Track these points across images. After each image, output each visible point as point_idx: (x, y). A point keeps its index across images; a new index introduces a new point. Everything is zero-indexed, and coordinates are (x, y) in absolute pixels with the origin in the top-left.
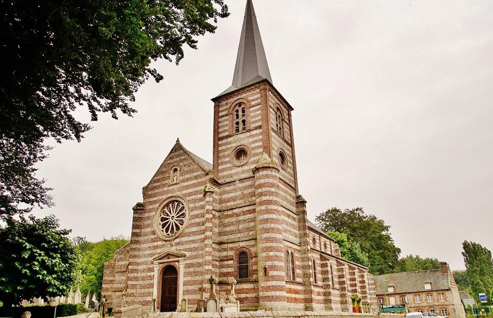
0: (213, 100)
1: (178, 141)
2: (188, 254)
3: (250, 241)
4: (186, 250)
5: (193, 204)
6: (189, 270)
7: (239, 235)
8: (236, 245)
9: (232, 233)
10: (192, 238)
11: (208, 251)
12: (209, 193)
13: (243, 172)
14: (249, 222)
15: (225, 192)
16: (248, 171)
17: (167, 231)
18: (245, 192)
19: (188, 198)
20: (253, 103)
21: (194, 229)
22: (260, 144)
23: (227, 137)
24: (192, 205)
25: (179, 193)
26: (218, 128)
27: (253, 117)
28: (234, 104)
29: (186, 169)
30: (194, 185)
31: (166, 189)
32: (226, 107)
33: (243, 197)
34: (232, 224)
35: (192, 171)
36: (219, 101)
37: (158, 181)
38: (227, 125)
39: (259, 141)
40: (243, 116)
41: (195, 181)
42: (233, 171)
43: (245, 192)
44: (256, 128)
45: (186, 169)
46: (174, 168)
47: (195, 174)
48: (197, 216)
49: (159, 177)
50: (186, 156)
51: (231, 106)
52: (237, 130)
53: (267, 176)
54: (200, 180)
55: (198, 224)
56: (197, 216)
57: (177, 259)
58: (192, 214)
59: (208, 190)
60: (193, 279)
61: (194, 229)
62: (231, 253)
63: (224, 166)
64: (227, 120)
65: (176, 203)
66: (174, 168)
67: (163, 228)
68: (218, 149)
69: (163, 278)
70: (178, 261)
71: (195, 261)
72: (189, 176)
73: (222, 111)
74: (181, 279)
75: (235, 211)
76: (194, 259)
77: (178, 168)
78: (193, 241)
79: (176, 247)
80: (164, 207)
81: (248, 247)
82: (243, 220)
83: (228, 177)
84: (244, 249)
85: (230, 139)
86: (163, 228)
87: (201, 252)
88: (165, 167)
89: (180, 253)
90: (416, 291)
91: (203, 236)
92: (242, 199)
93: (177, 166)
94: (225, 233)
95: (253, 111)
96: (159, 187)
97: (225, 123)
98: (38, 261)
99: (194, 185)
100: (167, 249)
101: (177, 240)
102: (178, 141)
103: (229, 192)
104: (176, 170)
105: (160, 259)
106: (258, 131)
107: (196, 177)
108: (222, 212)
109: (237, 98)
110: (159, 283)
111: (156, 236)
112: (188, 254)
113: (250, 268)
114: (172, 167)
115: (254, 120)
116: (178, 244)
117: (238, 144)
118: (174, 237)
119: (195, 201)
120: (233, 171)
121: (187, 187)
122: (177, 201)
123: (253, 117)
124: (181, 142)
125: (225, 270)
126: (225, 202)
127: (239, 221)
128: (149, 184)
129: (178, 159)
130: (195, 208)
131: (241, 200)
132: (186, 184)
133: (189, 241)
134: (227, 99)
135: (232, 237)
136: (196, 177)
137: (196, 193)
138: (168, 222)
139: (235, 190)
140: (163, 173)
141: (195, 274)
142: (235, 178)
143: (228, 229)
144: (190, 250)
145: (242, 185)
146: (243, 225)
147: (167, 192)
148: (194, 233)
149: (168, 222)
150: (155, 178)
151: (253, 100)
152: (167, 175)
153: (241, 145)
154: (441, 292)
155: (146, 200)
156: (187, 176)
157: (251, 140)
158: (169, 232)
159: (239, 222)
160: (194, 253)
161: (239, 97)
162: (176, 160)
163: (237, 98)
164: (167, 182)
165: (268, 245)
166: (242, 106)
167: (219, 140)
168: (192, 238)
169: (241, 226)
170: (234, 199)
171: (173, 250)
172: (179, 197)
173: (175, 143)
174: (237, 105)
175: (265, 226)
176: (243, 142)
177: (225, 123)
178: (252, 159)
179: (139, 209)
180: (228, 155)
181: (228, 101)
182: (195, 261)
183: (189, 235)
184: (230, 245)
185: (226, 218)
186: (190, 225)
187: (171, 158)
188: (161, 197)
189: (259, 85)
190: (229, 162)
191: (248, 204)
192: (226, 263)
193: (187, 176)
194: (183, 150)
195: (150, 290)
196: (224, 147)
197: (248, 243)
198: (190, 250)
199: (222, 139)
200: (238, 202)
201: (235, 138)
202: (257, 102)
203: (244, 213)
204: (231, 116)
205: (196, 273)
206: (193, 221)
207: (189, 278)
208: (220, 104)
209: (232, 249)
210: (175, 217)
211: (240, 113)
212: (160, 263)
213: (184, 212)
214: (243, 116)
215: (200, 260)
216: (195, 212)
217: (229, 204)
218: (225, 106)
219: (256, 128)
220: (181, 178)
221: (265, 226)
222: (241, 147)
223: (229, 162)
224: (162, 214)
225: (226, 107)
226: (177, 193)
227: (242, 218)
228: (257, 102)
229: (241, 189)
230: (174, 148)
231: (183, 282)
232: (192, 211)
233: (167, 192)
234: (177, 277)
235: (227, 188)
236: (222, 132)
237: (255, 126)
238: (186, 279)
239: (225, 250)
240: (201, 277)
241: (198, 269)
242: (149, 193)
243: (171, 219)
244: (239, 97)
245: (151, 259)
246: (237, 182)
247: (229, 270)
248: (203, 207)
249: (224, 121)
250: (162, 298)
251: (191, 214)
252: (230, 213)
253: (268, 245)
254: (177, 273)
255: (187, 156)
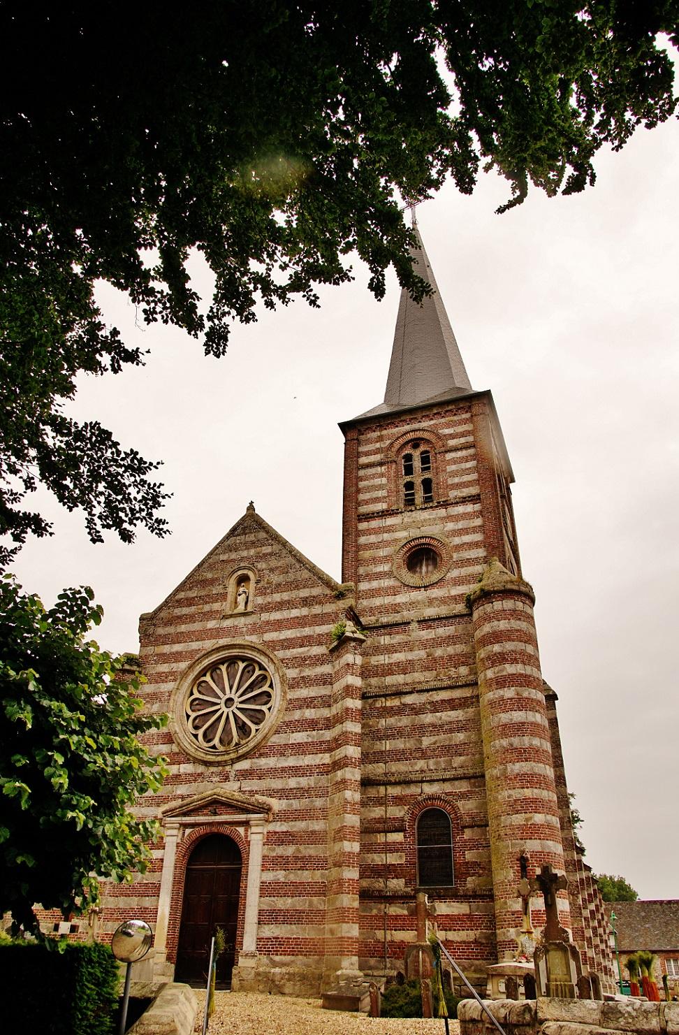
0: (345, 427)
1: (251, 507)
2: (276, 804)
3: (456, 783)
4: (271, 793)
5: (297, 670)
6: (280, 851)
7: (421, 764)
8: (414, 790)
9: (399, 756)
10: (291, 762)
11: (349, 799)
12: (353, 644)
13: (431, 602)
14: (451, 731)
15: (378, 650)
16: (455, 599)
17: (207, 738)
18: (439, 652)
19: (281, 654)
20: (452, 443)
21: (299, 737)
22: (478, 537)
23: (383, 514)
24: (292, 673)
25: (253, 639)
26: (358, 491)
27: (454, 474)
28: (401, 441)
29: (276, 578)
30: (301, 622)
31: (211, 624)
32: (378, 445)
33: (431, 664)
34: (398, 733)
35: (296, 586)
36: (359, 430)
37: (190, 602)
38: (380, 487)
39: (474, 530)
40: (423, 469)
41: (305, 611)
42: (400, 599)
43: (439, 652)
44: (464, 500)
45: (276, 578)
46: (240, 573)
47: (304, 593)
48: (309, 703)
49: (191, 594)
50: (276, 548)
51: (392, 444)
52: (410, 502)
53: (499, 615)
54: (317, 610)
55: (312, 725)
56: (309, 703)
57: (243, 817)
58: (292, 695)
59: (351, 635)
60: (292, 877)
61: (299, 737)
62: (396, 812)
63: (375, 584)
64: (382, 475)
65: (242, 665)
66: (240, 573)
67: (196, 728)
68: (356, 541)
69: (188, 870)
70: (246, 824)
71: (300, 825)
72: (286, 596)
73: (367, 454)
74: (255, 876)
75: (408, 699)
76: (295, 819)
77: (251, 574)
78: (296, 771)
79: (237, 785)
80: (203, 673)
81: (450, 798)
82: (434, 726)
83: (387, 612)
84: (437, 802)
85: (390, 521)
86: (196, 728)
87: (319, 803)
88: (211, 568)
89: (253, 799)
90: (668, 948)
91: (326, 758)
92: (427, 669)
93: (249, 569)
94: (380, 757)
95: (454, 461)
96: (191, 618)
97: (377, 481)
98: (63, 748)
99: (301, 622)
100: (211, 786)
101: (244, 765)
102: (251, 507)
103: (391, 649)
104: (243, 579)
105: (185, 814)
106: (470, 508)
107: (306, 602)
108: (370, 701)
109: (407, 428)
110: (175, 883)
111: (175, 748)
112: (276, 804)
113: (457, 858)
114: (234, 572)
115: (456, 480)
116: (245, 775)
117: (415, 533)
118: (233, 756)
119: (301, 662)
120: (400, 599)
121: (279, 625)
122: (243, 659)
123: (454, 474)
124: (259, 511)
125: (378, 859)
126: (376, 675)
127: (422, 727)
128: (160, 609)
129: (252, 552)
130: (305, 681)
131: (427, 674)
132: (276, 616)
133: (283, 770)
134: (381, 427)
135: (398, 767)
136: (306, 602)
137: (319, 640)
138: (217, 711)
139: (408, 646)
140: (205, 583)
141: (300, 864)
142: (406, 615)
143: (388, 745)
144: (283, 794)
145: (426, 634)
146: (433, 739)
147: (218, 633)
148: (300, 749)
149: (217, 711)
150: (182, 595)
151: (452, 436)
152: (216, 590)
153: (423, 537)
154: (672, 955)
155: (150, 650)
156: (277, 597)
157: (450, 526)
158: (216, 741)
159: (421, 730)
160: (296, 804)
161: (416, 426)
162: (245, 554)
163: (407, 428)
164: (216, 606)
165: (528, 793)
166: (422, 448)
167: (360, 520)
168: (291, 762)
169: (426, 741)
170: (404, 668)
171: (230, 789)
172: (253, 648)
173: (244, 512)
174: (407, 443)
175: (516, 741)
176: (428, 530)
177: (377, 481)
178: (455, 573)
179: (532, 589)
180: (386, 559)
181: (384, 432)
182: (300, 825)
183: (282, 751)
184: (394, 791)
185: (380, 716)
186: (287, 724)
187: (230, 549)
188: (195, 645)
189: (468, 404)
190: (389, 574)
191: (447, 683)
192: (381, 838)
193: (277, 597)
194: (267, 532)
195: (147, 902)
196: (373, 539)
197: (448, 787)
198: (283, 794)
199: (368, 517)
200: (418, 676)
201: (407, 517)
202: (463, 440)
203: (436, 707)
204: (394, 466)
205: (303, 863)
206: (297, 715)
207: (281, 875)
208: (362, 437)
209: (399, 801)
210: (236, 704)
211: (417, 464)
212: (185, 826)
213: (266, 688)
214: (423, 469)
215: (317, 826)
216: (304, 693)
217: (389, 680)
218: (373, 445)
219: (464, 500)
220: (260, 600)
221: (516, 741)
222: (423, 541)
223: (389, 574)
224: (195, 691)
225: (378, 445)
226: (247, 638)
227: (428, 718)
228: (463, 440)
229: (424, 644)
230: (238, 524)
231: (258, 884)
232: (292, 687)
233: (218, 633)
234: (240, 870)
235: (385, 640)
236: (367, 502)
237: (461, 495)
238: (269, 876)
239: (381, 802)
240: (318, 873)
241: (310, 851)
242: (161, 631)
243: (223, 705)
244: (416, 426)
245: (159, 811)
246: (414, 625)
247: (393, 859)
248: (326, 680)
249: (374, 476)
250: (181, 928)
251: (289, 697)
252: (395, 702)
253: (528, 793)
254: (240, 858)
255: (280, 547)
